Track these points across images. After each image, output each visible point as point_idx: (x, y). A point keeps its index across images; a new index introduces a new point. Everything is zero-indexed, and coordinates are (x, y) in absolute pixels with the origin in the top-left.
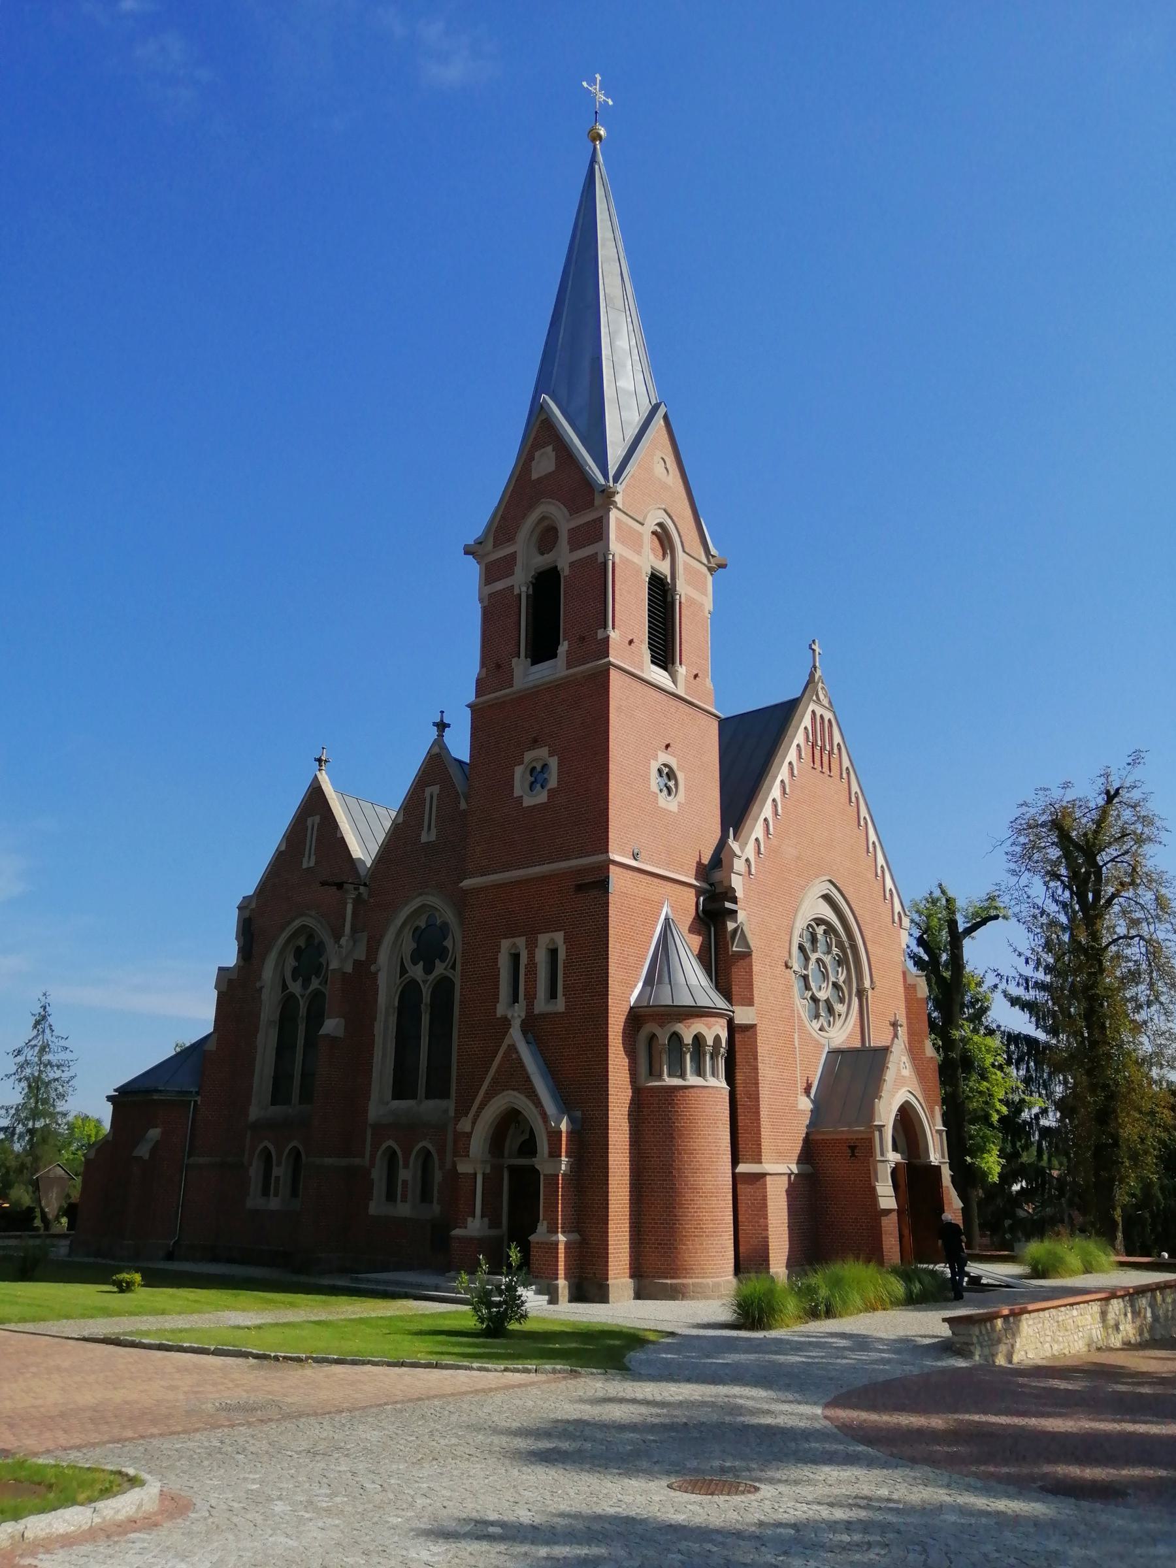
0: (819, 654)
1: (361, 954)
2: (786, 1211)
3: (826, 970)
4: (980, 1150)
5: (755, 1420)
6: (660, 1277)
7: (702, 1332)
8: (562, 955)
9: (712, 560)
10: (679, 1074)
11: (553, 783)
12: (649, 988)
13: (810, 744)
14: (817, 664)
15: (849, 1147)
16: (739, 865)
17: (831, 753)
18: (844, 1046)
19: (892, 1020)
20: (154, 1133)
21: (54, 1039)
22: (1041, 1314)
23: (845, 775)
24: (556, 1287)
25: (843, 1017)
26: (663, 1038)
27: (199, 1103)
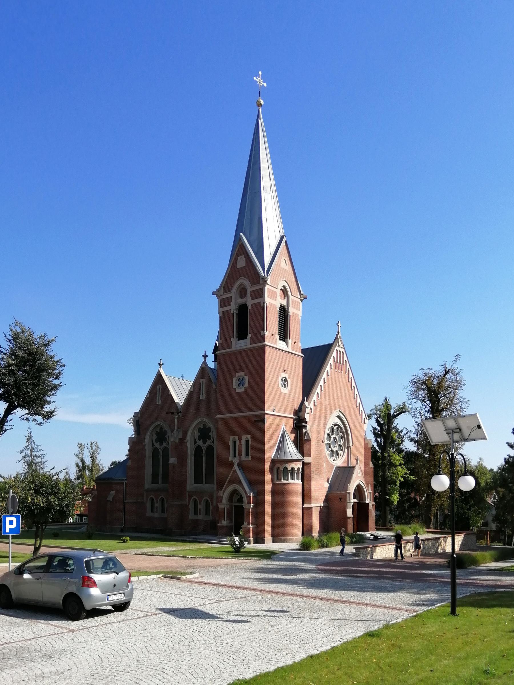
1: (180, 436)
5: (299, 568)
6: (280, 537)
8: (250, 443)
9: (302, 296)
11: (246, 385)
12: (278, 453)
13: (335, 362)
14: (339, 331)
16: (308, 410)
17: (343, 364)
18: (342, 466)
19: (356, 458)
20: (113, 493)
21: (35, 446)
22: (383, 547)
23: (347, 372)
24: (250, 540)
25: (342, 456)
26: (282, 469)
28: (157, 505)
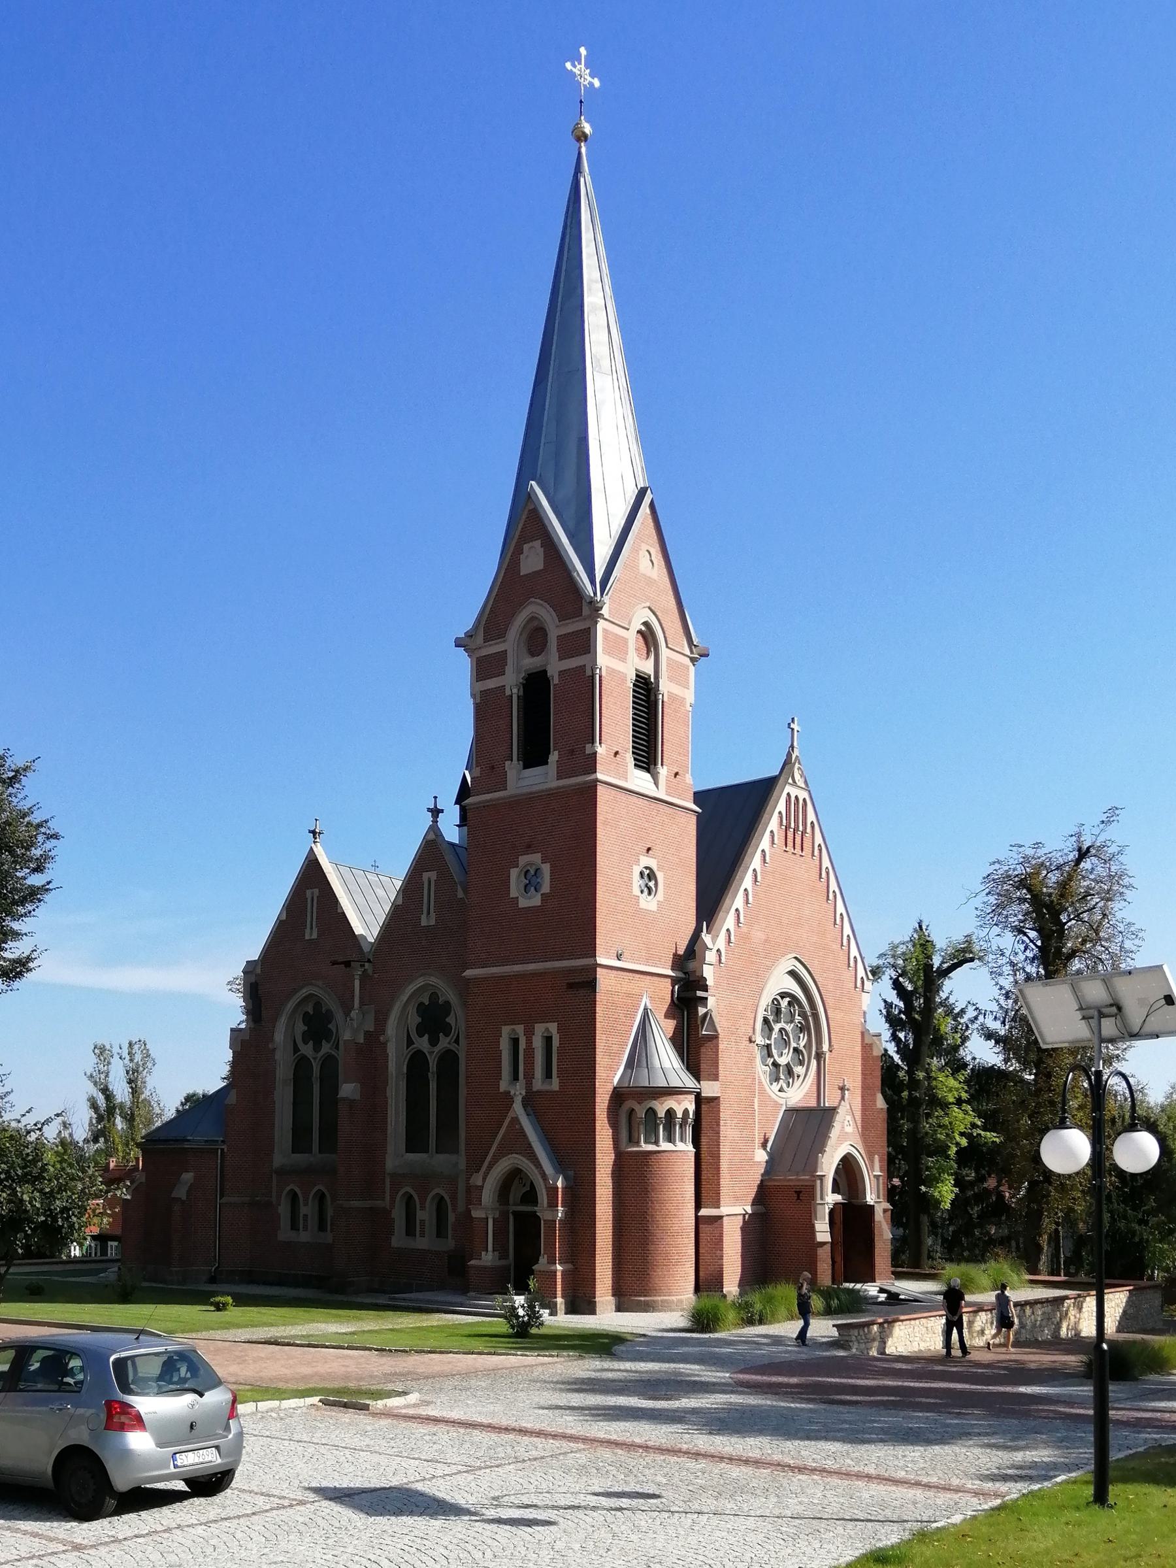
0: (798, 731)
1: (370, 1026)
2: (740, 1243)
3: (789, 1038)
4: (932, 1181)
6: (636, 1296)
7: (666, 1334)
8: (556, 1043)
9: (694, 650)
10: (653, 1141)
11: (546, 888)
13: (784, 827)
14: (795, 744)
15: (796, 1192)
16: (710, 957)
17: (804, 832)
19: (841, 1085)
20: (188, 1177)
24: (556, 1304)
26: (641, 1113)
27: (226, 1150)
28: (307, 1210)
